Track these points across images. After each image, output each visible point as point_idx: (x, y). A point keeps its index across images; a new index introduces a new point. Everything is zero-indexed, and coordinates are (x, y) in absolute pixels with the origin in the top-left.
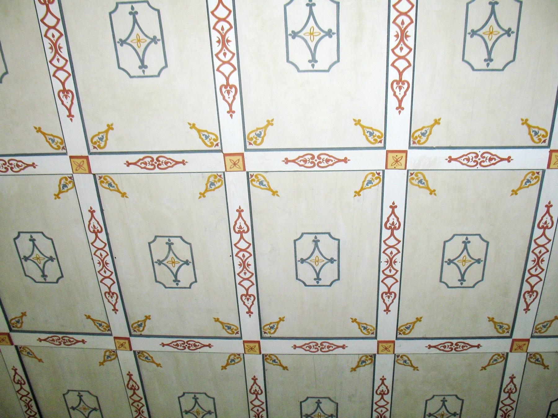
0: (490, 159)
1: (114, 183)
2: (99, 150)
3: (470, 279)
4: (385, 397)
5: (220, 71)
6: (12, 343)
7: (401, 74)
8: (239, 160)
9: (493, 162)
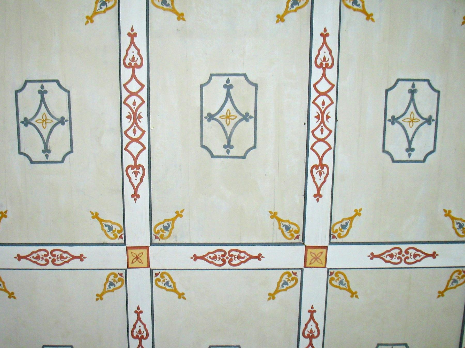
0: (215, 258)
1: (282, 231)
7: (133, 76)
8: (132, 263)
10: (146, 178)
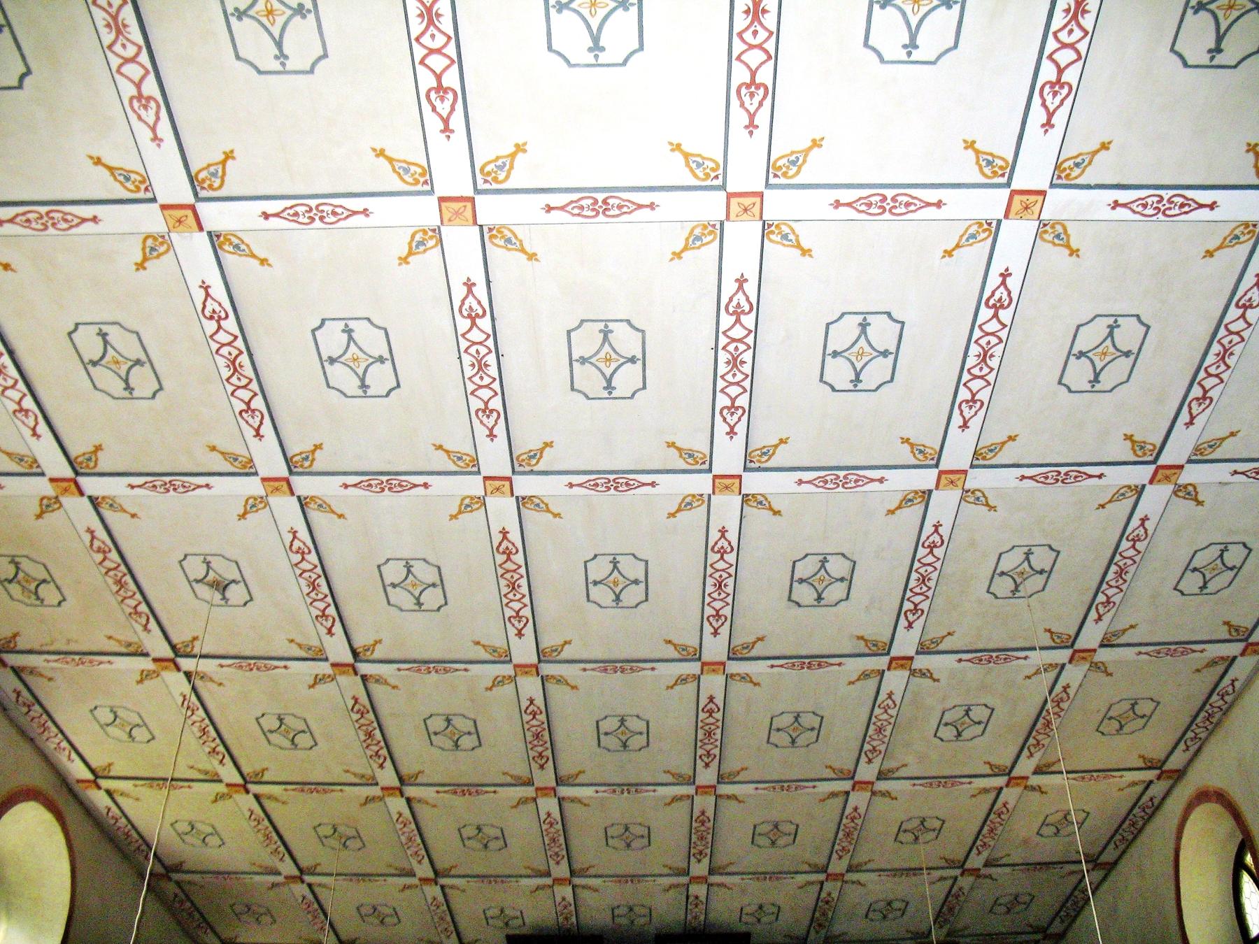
0: (1182, 205)
1: (516, 237)
2: (495, 186)
3: (869, 380)
4: (936, 551)
5: (121, 74)
6: (81, 493)
7: (1061, 71)
9: (1186, 209)
10: (724, 301)
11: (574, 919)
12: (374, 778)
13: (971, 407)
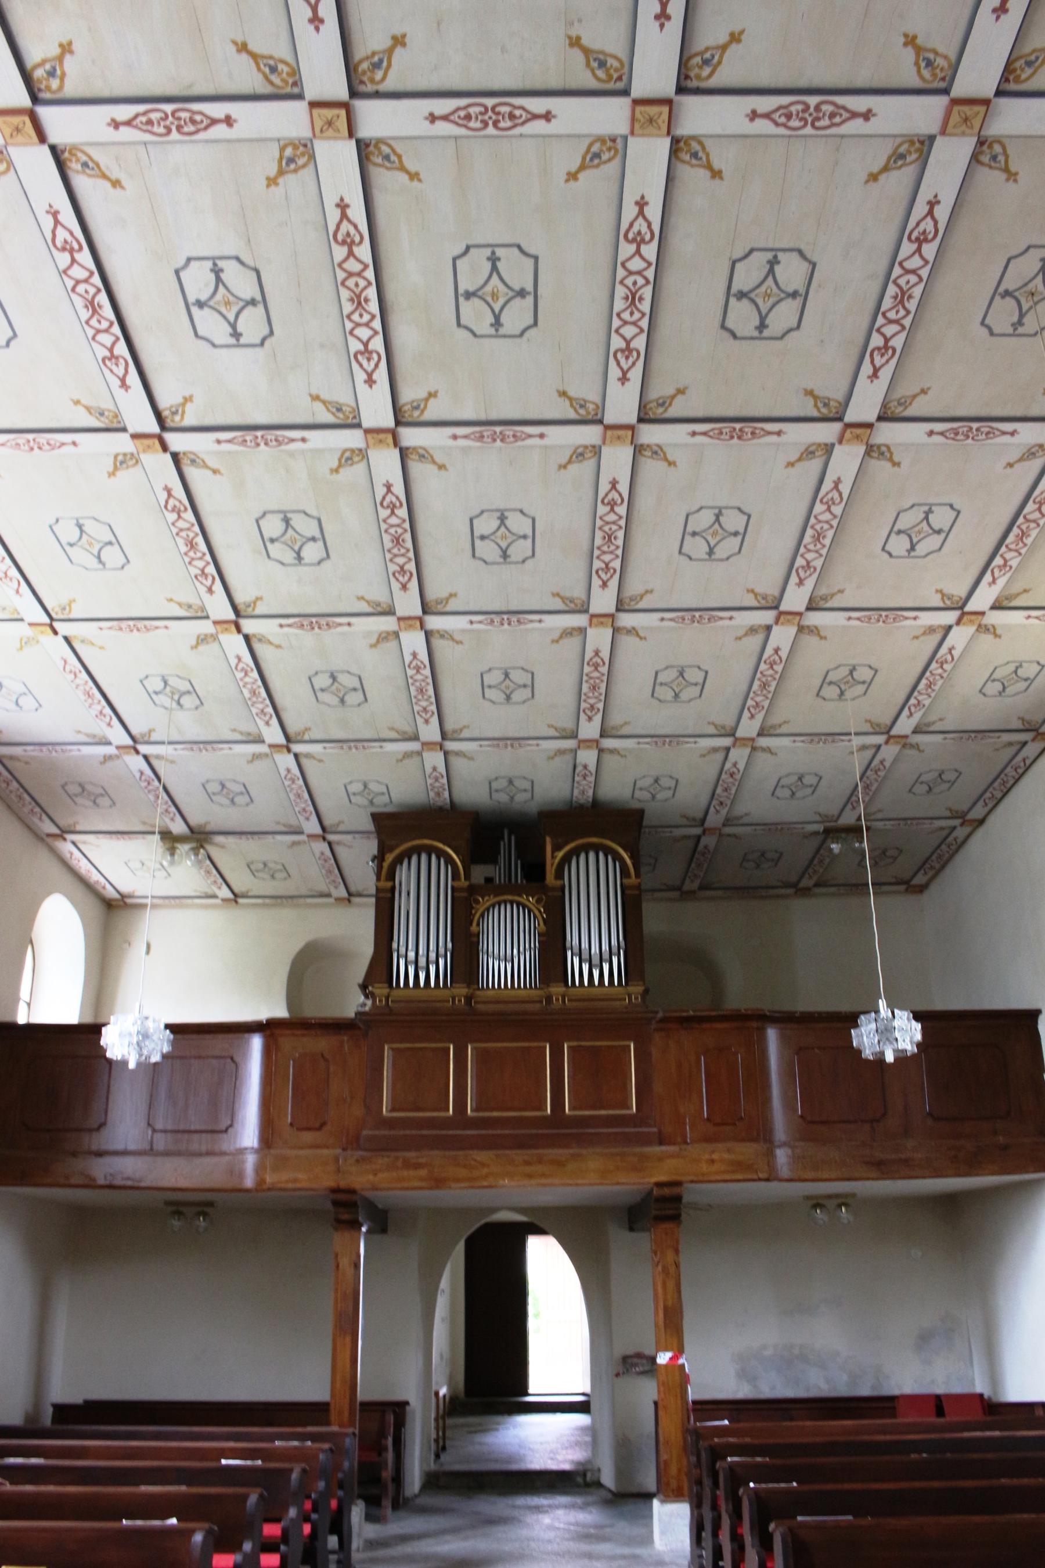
0: (832, 115)
11: (446, 794)
12: (203, 609)
13: (882, 355)
